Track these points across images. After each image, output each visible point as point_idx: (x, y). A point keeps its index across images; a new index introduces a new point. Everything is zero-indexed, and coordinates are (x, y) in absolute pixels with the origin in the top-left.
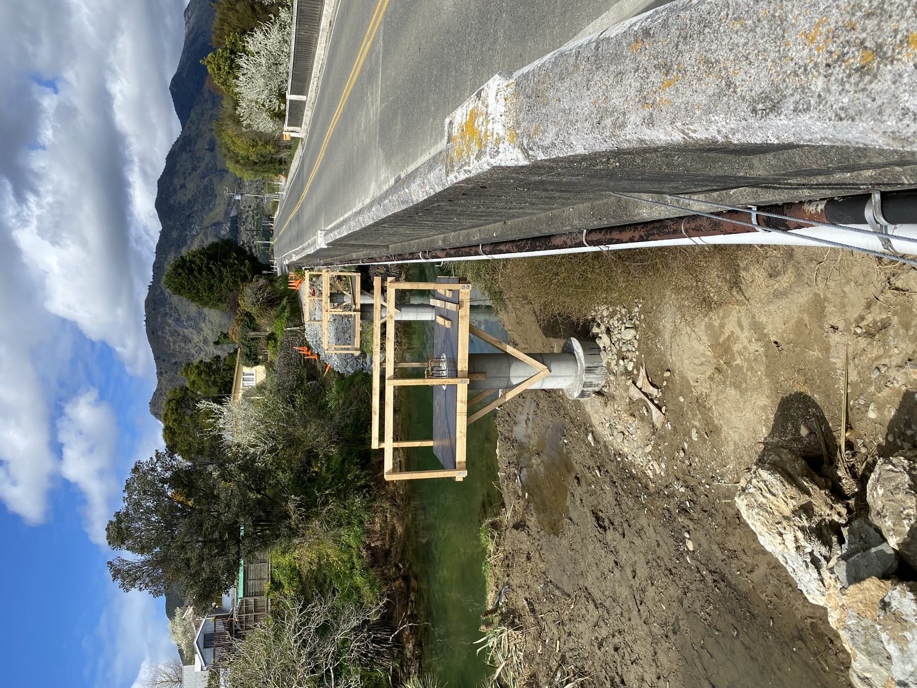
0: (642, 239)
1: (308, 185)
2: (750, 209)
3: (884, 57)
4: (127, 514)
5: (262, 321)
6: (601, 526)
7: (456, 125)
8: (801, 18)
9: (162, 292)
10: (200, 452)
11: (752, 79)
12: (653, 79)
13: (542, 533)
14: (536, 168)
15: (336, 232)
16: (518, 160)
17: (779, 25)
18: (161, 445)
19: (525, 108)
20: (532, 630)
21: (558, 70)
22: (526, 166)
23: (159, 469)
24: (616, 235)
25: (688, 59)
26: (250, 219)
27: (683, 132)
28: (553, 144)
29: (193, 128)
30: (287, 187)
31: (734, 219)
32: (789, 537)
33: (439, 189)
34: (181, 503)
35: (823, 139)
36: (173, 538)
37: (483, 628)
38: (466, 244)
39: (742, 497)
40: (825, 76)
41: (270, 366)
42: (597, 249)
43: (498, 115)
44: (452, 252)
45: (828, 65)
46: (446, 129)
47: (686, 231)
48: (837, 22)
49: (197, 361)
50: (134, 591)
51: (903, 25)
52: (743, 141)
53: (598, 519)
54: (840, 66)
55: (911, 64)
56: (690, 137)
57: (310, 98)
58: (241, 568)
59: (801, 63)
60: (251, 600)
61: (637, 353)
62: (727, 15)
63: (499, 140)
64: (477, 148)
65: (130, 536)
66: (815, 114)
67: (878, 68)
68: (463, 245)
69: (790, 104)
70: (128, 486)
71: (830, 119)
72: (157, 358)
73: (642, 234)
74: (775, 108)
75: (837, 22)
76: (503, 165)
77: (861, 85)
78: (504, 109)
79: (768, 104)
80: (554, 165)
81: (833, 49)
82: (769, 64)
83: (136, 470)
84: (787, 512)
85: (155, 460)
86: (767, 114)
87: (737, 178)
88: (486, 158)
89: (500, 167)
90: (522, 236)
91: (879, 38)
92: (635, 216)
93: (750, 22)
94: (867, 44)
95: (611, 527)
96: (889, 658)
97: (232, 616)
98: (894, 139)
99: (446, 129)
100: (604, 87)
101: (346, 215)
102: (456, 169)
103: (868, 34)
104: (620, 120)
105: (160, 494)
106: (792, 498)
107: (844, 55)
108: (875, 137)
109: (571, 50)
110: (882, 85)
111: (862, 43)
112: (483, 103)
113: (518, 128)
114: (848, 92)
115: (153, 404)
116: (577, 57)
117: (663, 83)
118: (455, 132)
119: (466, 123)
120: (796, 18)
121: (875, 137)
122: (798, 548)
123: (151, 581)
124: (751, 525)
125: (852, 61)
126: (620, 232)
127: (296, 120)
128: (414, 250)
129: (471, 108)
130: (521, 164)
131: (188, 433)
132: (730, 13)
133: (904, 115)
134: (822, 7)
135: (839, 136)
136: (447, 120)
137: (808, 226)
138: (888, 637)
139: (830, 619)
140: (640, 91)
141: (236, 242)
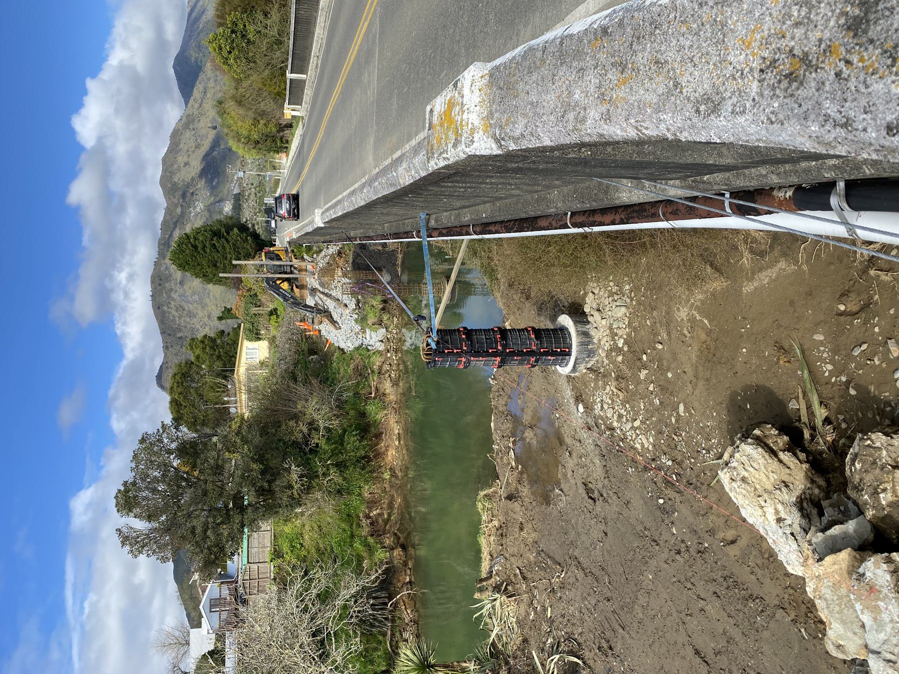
0: (622, 222)
1: (309, 163)
2: (723, 195)
3: (809, 65)
4: (134, 484)
5: (263, 298)
6: (590, 498)
7: (435, 113)
8: (739, 24)
9: (167, 268)
10: (204, 424)
11: (697, 81)
12: (610, 77)
13: (534, 503)
14: (510, 156)
15: (331, 212)
16: (492, 149)
17: (720, 30)
18: (168, 419)
19: (498, 100)
20: (525, 597)
21: (527, 64)
22: (500, 155)
23: (166, 441)
24: (598, 218)
25: (642, 58)
26: (252, 197)
27: (637, 129)
28: (522, 135)
29: (196, 106)
30: (289, 164)
31: (710, 205)
32: (770, 511)
33: (423, 174)
35: (758, 140)
36: (179, 507)
37: (477, 596)
38: (457, 224)
39: (725, 470)
40: (759, 81)
41: (272, 341)
42: (581, 230)
43: (473, 106)
44: (444, 231)
45: (762, 71)
46: (427, 116)
47: (664, 215)
48: (769, 30)
49: (202, 334)
50: (142, 557)
51: (827, 34)
52: (690, 139)
53: (588, 491)
54: (772, 72)
55: (833, 73)
56: (643, 134)
57: (310, 77)
58: (245, 536)
59: (739, 68)
60: (255, 567)
62: (676, 17)
63: (473, 131)
64: (454, 137)
65: (138, 504)
66: (749, 116)
67: (804, 75)
68: (454, 225)
69: (728, 106)
70: (135, 456)
71: (763, 123)
72: (163, 333)
73: (623, 217)
74: (715, 109)
75: (769, 30)
76: (478, 153)
77: (789, 91)
78: (479, 99)
79: (711, 104)
80: (527, 154)
81: (766, 55)
82: (711, 67)
83: (143, 441)
84: (770, 487)
85: (161, 431)
86: (709, 115)
87: (707, 166)
88: (462, 147)
89: (475, 156)
90: (510, 217)
91: (806, 46)
92: (616, 199)
93: (695, 26)
94: (795, 52)
95: (601, 499)
96: (863, 626)
98: (818, 143)
99: (427, 116)
100: (567, 82)
101: (340, 197)
102: (436, 156)
103: (796, 42)
104: (581, 115)
105: (166, 466)
106: (773, 472)
107: (775, 61)
108: (803, 140)
109: (538, 45)
110: (807, 91)
111: (791, 51)
112: (459, 93)
113: (492, 118)
114: (778, 97)
115: (159, 377)
116: (544, 52)
117: (619, 80)
118: (435, 120)
119: (445, 112)
120: (734, 24)
121: (803, 140)
122: (779, 520)
123: (159, 548)
124: (733, 498)
125: (782, 67)
126: (602, 214)
127: (296, 99)
128: (409, 229)
129: (448, 97)
130: (495, 153)
131: (193, 406)
132: (678, 15)
133: (825, 121)
134: (757, 14)
135: (772, 138)
136: (428, 108)
137: (770, 213)
138: (861, 607)
139: (807, 589)
140: (599, 87)
141: (238, 219)
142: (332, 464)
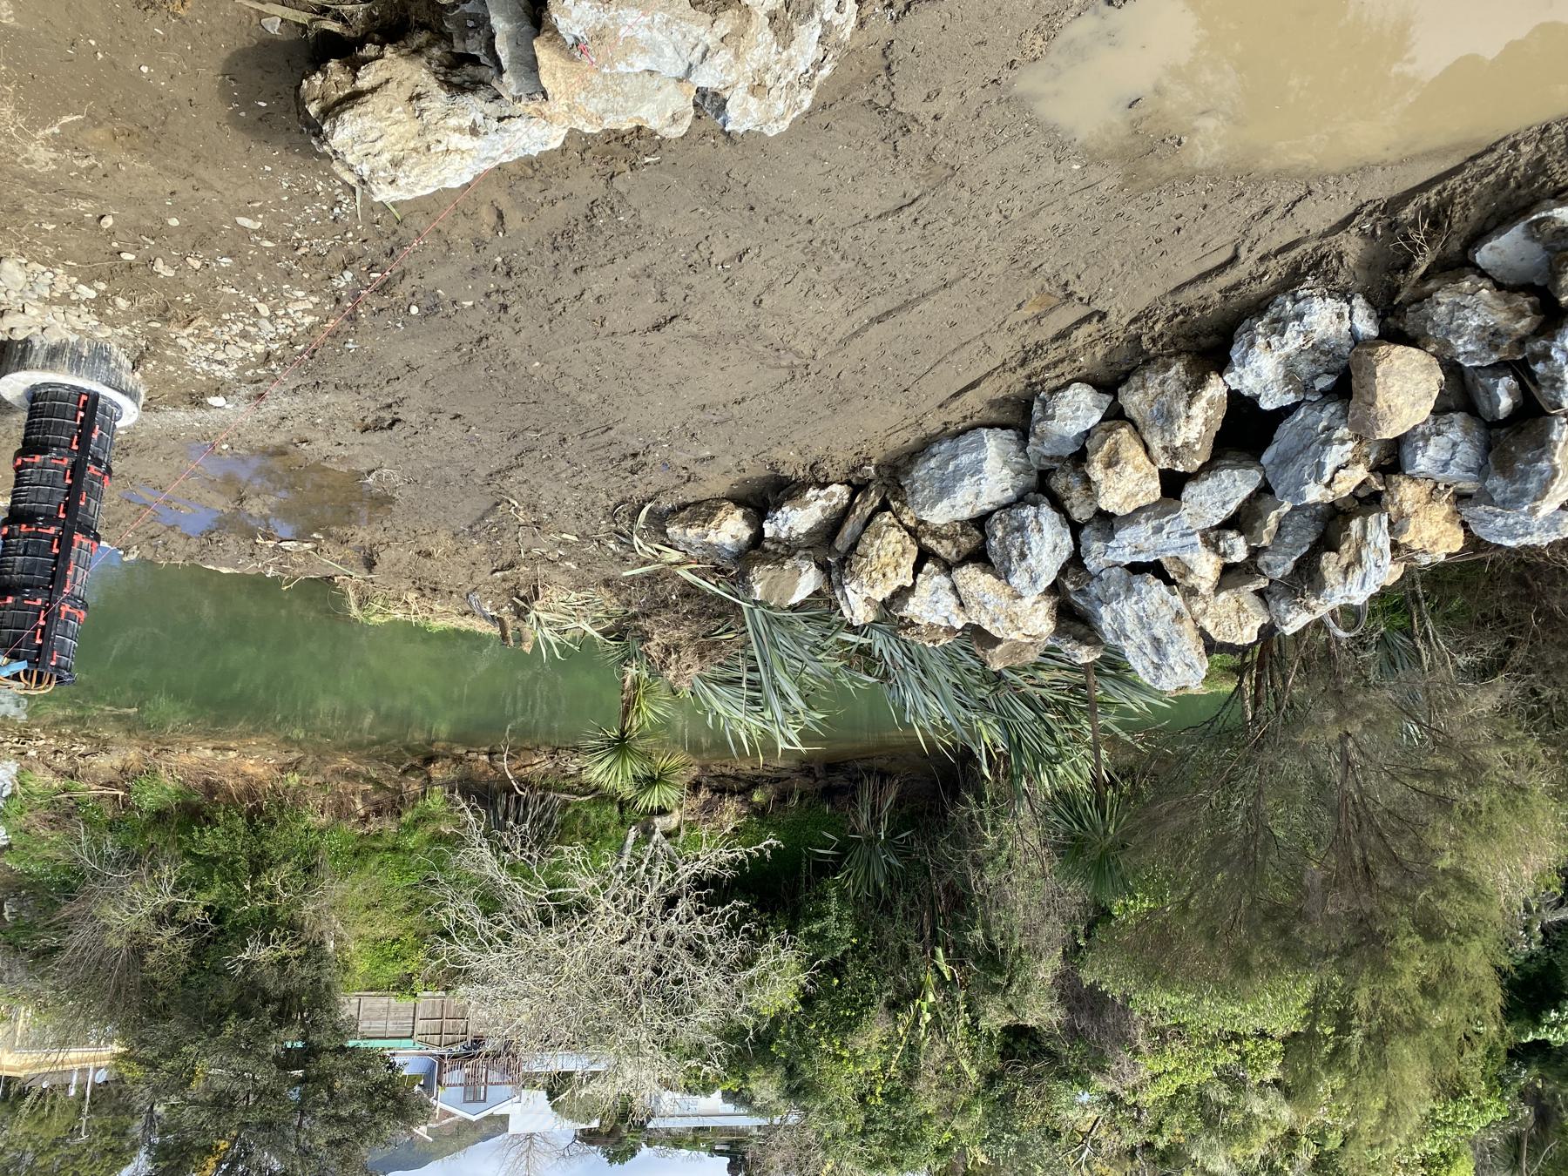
13: (387, 524)
20: (541, 570)
32: (456, 140)
34: (219, 1163)
39: (374, 188)
53: (377, 427)
61: (59, 271)
84: (416, 126)
95: (395, 409)
97: (442, 1056)
106: (390, 111)
142: (253, 881)
